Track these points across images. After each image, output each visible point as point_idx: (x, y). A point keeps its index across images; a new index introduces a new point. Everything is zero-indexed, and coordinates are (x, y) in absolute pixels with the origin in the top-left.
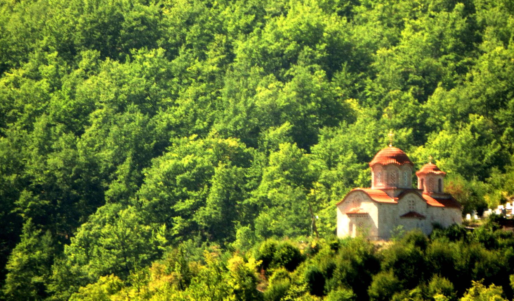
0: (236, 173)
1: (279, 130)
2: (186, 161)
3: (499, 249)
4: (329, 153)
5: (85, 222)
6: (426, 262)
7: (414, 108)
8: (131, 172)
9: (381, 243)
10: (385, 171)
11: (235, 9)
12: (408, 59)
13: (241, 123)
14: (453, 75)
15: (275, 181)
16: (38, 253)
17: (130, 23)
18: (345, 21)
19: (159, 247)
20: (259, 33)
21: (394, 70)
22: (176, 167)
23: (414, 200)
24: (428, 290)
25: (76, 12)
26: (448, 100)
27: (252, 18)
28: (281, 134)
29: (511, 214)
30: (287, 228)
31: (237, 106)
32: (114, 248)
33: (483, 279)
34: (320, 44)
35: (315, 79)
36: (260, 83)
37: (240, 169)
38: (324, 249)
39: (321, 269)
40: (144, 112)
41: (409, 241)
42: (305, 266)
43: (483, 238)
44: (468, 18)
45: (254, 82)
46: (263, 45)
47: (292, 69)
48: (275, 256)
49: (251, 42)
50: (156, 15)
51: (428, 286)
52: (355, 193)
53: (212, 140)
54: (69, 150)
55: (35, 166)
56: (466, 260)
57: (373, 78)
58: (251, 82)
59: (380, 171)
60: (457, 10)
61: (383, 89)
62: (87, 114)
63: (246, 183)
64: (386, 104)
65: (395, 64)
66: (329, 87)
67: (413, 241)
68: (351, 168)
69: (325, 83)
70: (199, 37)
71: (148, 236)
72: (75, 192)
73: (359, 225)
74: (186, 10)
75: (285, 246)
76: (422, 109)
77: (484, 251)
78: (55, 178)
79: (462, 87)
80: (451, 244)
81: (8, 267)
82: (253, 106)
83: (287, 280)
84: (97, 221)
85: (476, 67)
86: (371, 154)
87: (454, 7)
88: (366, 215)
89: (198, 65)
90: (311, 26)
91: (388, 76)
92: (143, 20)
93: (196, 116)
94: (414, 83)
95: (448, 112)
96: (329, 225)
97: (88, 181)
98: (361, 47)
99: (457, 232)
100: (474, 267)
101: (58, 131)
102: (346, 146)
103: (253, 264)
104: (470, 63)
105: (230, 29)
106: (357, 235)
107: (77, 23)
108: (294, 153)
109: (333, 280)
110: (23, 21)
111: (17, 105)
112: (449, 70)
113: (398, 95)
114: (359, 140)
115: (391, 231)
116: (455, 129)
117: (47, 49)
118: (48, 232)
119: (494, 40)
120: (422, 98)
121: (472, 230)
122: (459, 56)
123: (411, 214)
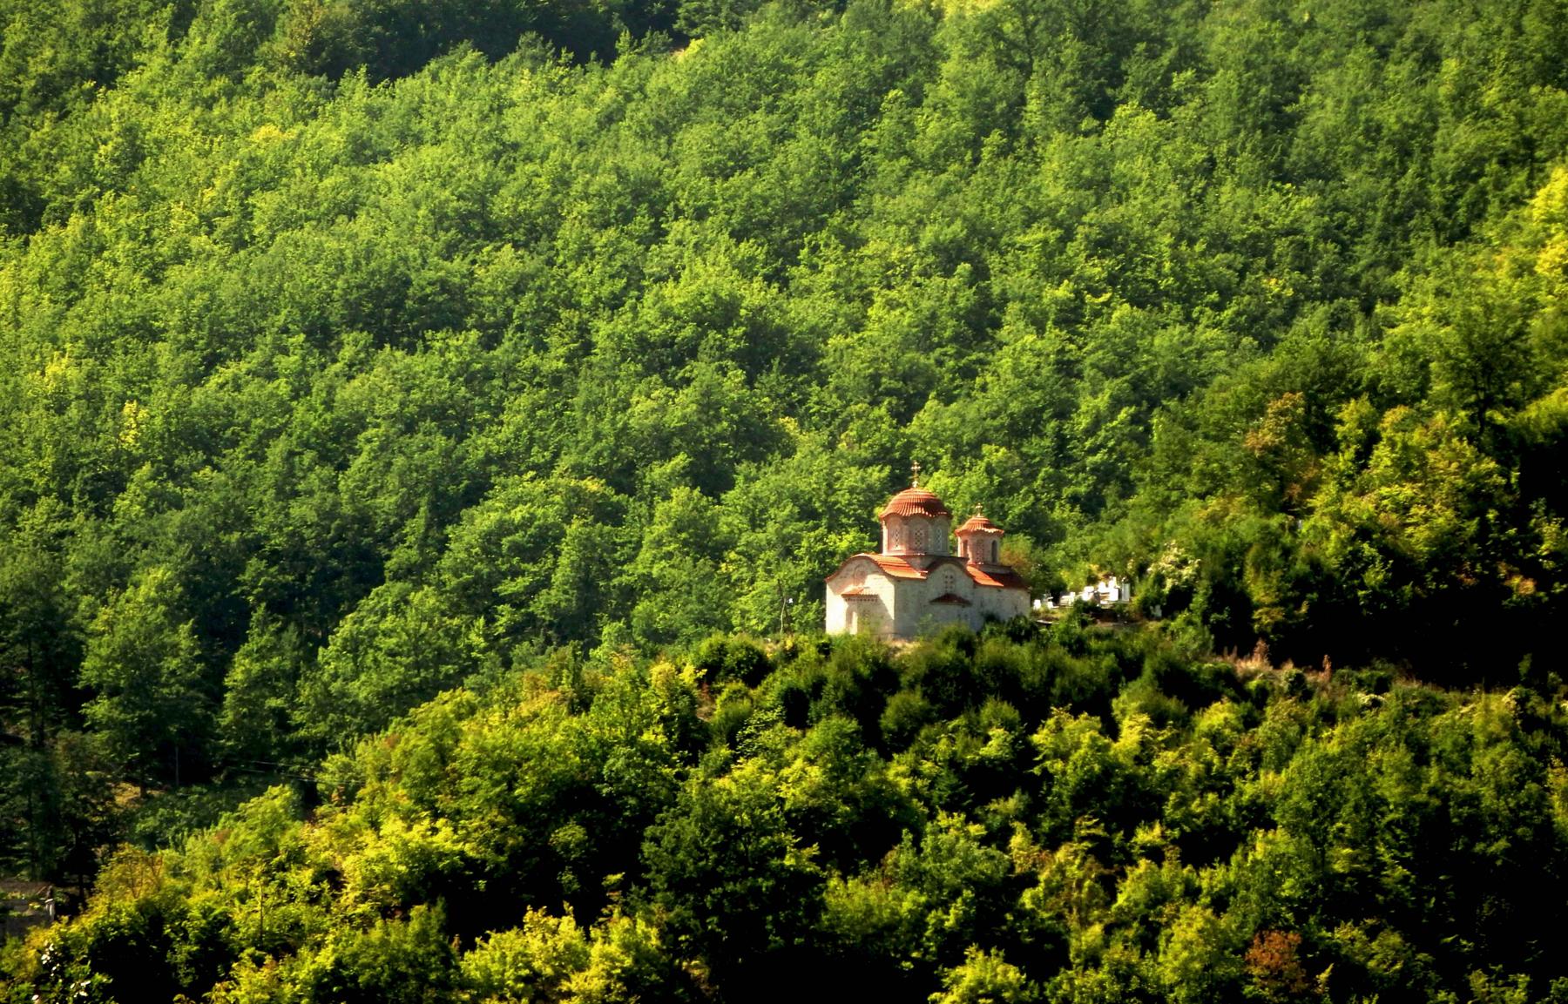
0: (601, 535)
1: (668, 467)
2: (518, 514)
5: (351, 611)
8: (427, 530)
9: (899, 644)
14: (953, 380)
15: (665, 549)
16: (275, 660)
17: (423, 289)
19: (474, 654)
20: (634, 309)
22: (501, 523)
25: (332, 270)
30: (683, 626)
31: (600, 426)
32: (400, 654)
35: (728, 384)
37: (607, 528)
39: (802, 684)
40: (448, 434)
41: (946, 641)
43: (1066, 638)
49: (622, 323)
50: (464, 276)
52: (857, 563)
53: (561, 480)
54: (326, 494)
55: (269, 519)
57: (823, 383)
58: (624, 388)
61: (839, 403)
62: (353, 434)
64: (844, 425)
67: (953, 642)
68: (789, 529)
70: (535, 313)
71: (455, 635)
72: (335, 563)
73: (863, 614)
74: (513, 270)
76: (903, 435)
77: (1069, 660)
78: (303, 540)
80: (1015, 647)
81: (228, 682)
82: (626, 426)
83: (746, 703)
84: (371, 611)
88: (874, 599)
89: (533, 359)
91: (848, 381)
92: (444, 285)
93: (532, 441)
94: (889, 392)
96: (754, 622)
97: (357, 546)
98: (801, 333)
101: (306, 462)
102: (779, 494)
104: (981, 362)
105: (586, 301)
106: (860, 630)
107: (334, 287)
109: (822, 703)
110: (246, 284)
111: (240, 420)
116: (958, 469)
117: (285, 330)
118: (292, 627)
119: (1021, 324)
123: (947, 598)
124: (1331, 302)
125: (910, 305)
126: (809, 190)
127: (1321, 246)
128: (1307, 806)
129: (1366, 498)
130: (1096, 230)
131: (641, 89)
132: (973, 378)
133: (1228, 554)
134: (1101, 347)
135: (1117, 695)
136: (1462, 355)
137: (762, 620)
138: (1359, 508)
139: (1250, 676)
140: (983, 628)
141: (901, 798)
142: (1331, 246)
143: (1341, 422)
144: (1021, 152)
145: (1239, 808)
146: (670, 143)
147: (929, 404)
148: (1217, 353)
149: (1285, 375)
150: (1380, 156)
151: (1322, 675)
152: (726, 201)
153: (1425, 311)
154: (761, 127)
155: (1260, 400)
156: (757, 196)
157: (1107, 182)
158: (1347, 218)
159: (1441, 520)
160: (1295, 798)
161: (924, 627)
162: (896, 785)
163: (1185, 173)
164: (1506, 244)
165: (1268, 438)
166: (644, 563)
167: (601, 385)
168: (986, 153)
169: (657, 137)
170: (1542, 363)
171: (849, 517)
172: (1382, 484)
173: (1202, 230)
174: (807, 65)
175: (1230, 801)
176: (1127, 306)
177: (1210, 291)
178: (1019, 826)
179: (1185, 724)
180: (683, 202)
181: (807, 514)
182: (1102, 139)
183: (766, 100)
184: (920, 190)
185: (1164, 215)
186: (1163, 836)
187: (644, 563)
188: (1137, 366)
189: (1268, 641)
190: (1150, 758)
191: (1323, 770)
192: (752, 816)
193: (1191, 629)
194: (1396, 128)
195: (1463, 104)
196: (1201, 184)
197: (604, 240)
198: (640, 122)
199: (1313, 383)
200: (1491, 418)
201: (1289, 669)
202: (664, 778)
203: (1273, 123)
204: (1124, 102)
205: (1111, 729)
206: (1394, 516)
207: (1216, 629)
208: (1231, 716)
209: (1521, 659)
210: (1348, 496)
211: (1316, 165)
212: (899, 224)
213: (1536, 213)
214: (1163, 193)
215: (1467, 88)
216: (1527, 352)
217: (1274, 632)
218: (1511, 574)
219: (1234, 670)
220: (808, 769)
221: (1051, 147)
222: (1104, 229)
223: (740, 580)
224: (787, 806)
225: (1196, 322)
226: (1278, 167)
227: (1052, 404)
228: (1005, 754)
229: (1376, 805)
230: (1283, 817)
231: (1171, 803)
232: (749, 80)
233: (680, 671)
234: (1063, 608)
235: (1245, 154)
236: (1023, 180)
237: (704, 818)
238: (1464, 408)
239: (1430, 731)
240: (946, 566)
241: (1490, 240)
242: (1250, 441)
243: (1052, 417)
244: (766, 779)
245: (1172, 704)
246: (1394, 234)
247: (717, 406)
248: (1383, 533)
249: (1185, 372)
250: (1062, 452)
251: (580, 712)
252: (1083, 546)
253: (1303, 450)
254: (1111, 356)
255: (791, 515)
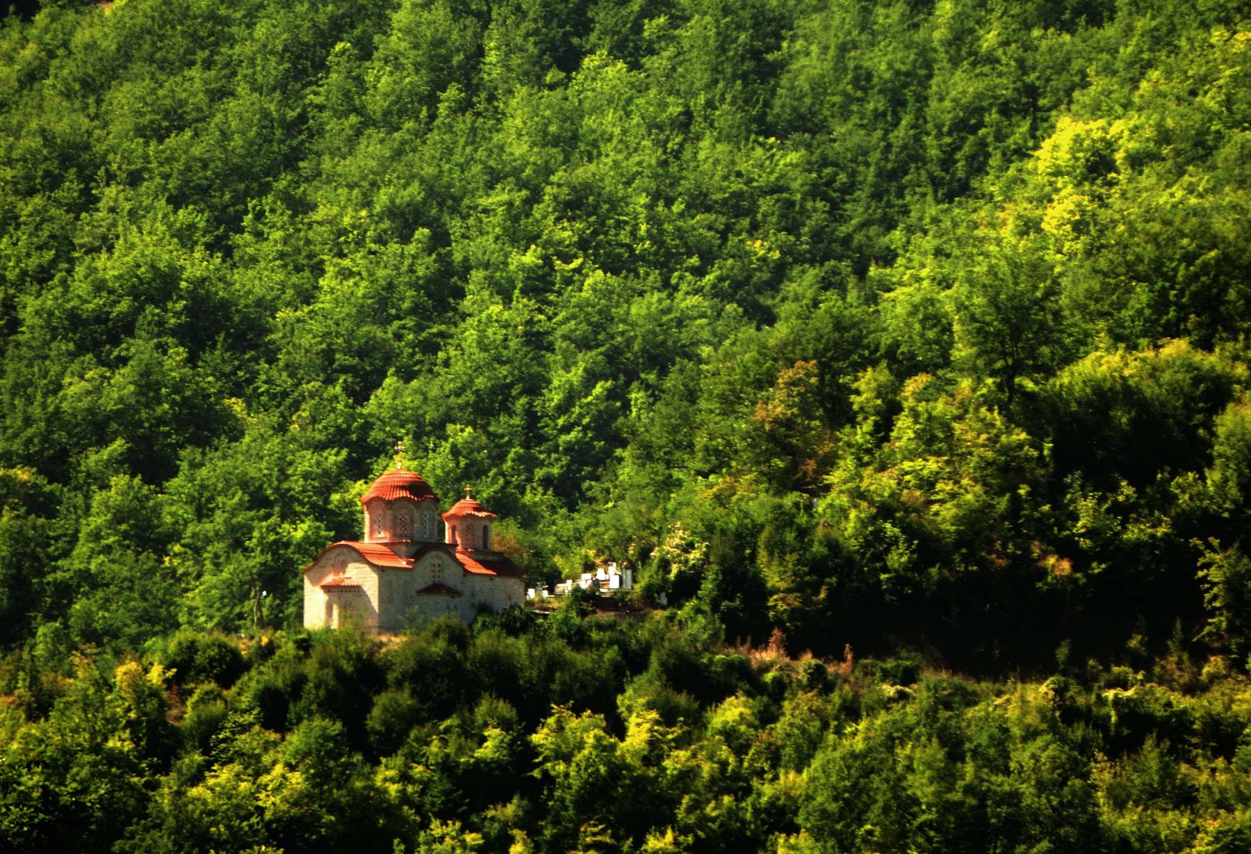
0: (34, 528)
1: (105, 453)
9: (384, 639)
10: (390, 512)
11: (18, 240)
13: (36, 440)
14: (412, 355)
15: (104, 542)
18: (219, 261)
20: (64, 282)
24: (473, 722)
27: (50, 255)
28: (109, 460)
31: (30, 410)
34: (176, 302)
35: (168, 363)
36: (69, 370)
37: (41, 521)
41: (436, 635)
42: (250, 679)
44: (439, 255)
45: (58, 368)
46: (72, 304)
47: (124, 346)
52: (337, 551)
57: (272, 361)
58: (54, 369)
60: (419, 241)
61: (290, 381)
63: (49, 545)
64: (296, 406)
66: (194, 376)
67: (444, 636)
68: (240, 518)
69: (187, 369)
73: (344, 607)
75: (214, 644)
76: (361, 415)
77: (569, 653)
80: (511, 640)
82: (58, 409)
83: (220, 704)
85: (454, 341)
87: (412, 235)
88: (357, 590)
90: (159, 269)
91: (299, 357)
94: (344, 370)
95: (407, 421)
96: (202, 619)
98: (246, 306)
104: (441, 335)
105: (11, 275)
106: (342, 623)
109: (302, 703)
112: (407, 345)
114: (253, 471)
115: (400, 617)
119: (486, 294)
120: (360, 395)
123: (436, 588)
124: (822, 264)
125: (364, 274)
126: (253, 149)
127: (809, 205)
128: (833, 807)
129: (886, 473)
130: (565, 190)
131: (65, 44)
133: (738, 535)
134: (574, 317)
135: (623, 691)
136: (988, 318)
138: (882, 483)
139: (766, 668)
140: (475, 620)
141: (391, 806)
142: (820, 204)
143: (858, 392)
144: (480, 107)
145: (757, 811)
146: (99, 102)
147: (387, 381)
148: (699, 322)
149: (796, 342)
150: (871, 106)
151: (843, 665)
152: (161, 164)
153: (924, 273)
154: (198, 84)
155: (769, 369)
156: (195, 159)
157: (575, 138)
158: (836, 174)
159: (969, 497)
160: (820, 799)
162: (386, 791)
163: (660, 128)
164: (1009, 199)
165: (779, 410)
166: (82, 558)
167: (30, 365)
168: (442, 109)
169: (84, 96)
170: (1075, 325)
172: (905, 458)
173: (680, 189)
174: (245, 16)
175: (747, 804)
176: (600, 273)
177: (690, 255)
178: (518, 833)
179: (697, 722)
180: (115, 167)
181: (258, 501)
182: (569, 92)
183: (202, 55)
184: (372, 149)
185: (638, 173)
186: (676, 843)
187: (82, 558)
188: (612, 337)
189: (784, 630)
190: (660, 758)
191: (849, 768)
192: (229, 827)
193: (700, 618)
194: (887, 75)
195: (959, 50)
196: (678, 140)
197: (30, 208)
198: (64, 80)
199: (826, 350)
200: (1021, 386)
201: (808, 659)
202: (132, 787)
203: (753, 71)
204: (592, 52)
205: (617, 728)
206: (918, 493)
207: (727, 617)
208: (747, 711)
209: (1058, 645)
210: (869, 471)
211: (802, 117)
212: (351, 187)
213: (1041, 166)
214: (636, 150)
215: (963, 32)
216: (1057, 315)
217: (790, 620)
218: (1045, 554)
219: (749, 661)
220: (289, 775)
221: (514, 103)
222: (574, 189)
223: (186, 574)
224: (268, 815)
225: (676, 288)
226: (760, 119)
227: (520, 379)
228: (503, 755)
229: (905, 805)
230: (807, 819)
231: (684, 806)
232: (183, 32)
233: (146, 671)
234: (559, 597)
235: (725, 107)
236: (484, 138)
237: (177, 831)
238: (991, 376)
239: (964, 724)
240: (434, 553)
241: (992, 196)
242: (760, 413)
244: (244, 786)
245: (682, 699)
246: (887, 191)
247: (156, 386)
248: (907, 511)
249: (664, 343)
250: (533, 432)
251: (38, 718)
252: (577, 530)
253: (817, 423)
254: (584, 326)
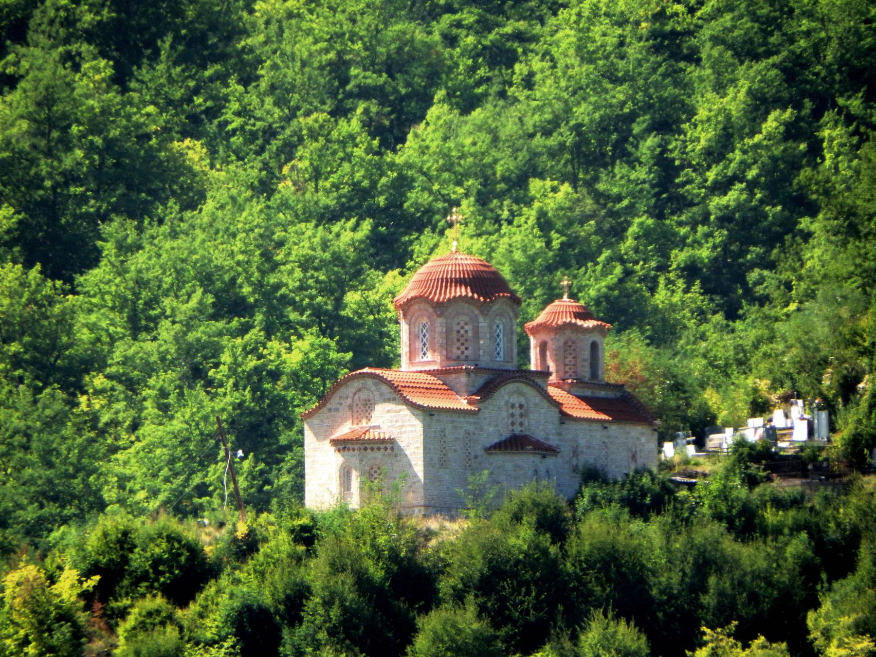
3: (770, 538)
4: (134, 294)
6: (568, 574)
7: (370, 163)
9: (433, 524)
12: (347, 26)
14: (473, 69)
21: (305, 55)
23: (522, 400)
26: (468, 141)
29: (792, 442)
33: (735, 623)
35: (82, 85)
38: (272, 543)
39: (267, 599)
41: (517, 518)
42: (219, 591)
43: (723, 508)
47: (11, 57)
48: (135, 564)
51: (575, 645)
52: (356, 384)
56: (682, 570)
59: (425, 320)
61: (277, 113)
64: (288, 151)
65: (310, 39)
66: (123, 105)
67: (529, 519)
73: (370, 474)
75: (160, 535)
76: (392, 166)
77: (730, 546)
79: (501, 103)
80: (637, 525)
83: (171, 632)
86: (253, 293)
88: (388, 446)
91: (291, 74)
94: (365, 93)
95: (466, 175)
96: (141, 495)
99: (650, 490)
100: (705, 591)
103: (73, 586)
104: (519, 36)
108: (33, 293)
109: (302, 630)
112: (462, 55)
113: (322, 127)
115: (459, 490)
121: (691, 486)
122: (491, 17)
132: (510, 65)
135: (817, 605)
137: (154, 493)
147: (433, 112)
161: (478, 495)
171: (301, 311)
188: (792, 40)
227: (648, 107)
234: (713, 455)
240: (511, 387)
243: (648, 131)
247: (62, 122)
252: (739, 348)
254: (747, 23)
255: (201, 308)
